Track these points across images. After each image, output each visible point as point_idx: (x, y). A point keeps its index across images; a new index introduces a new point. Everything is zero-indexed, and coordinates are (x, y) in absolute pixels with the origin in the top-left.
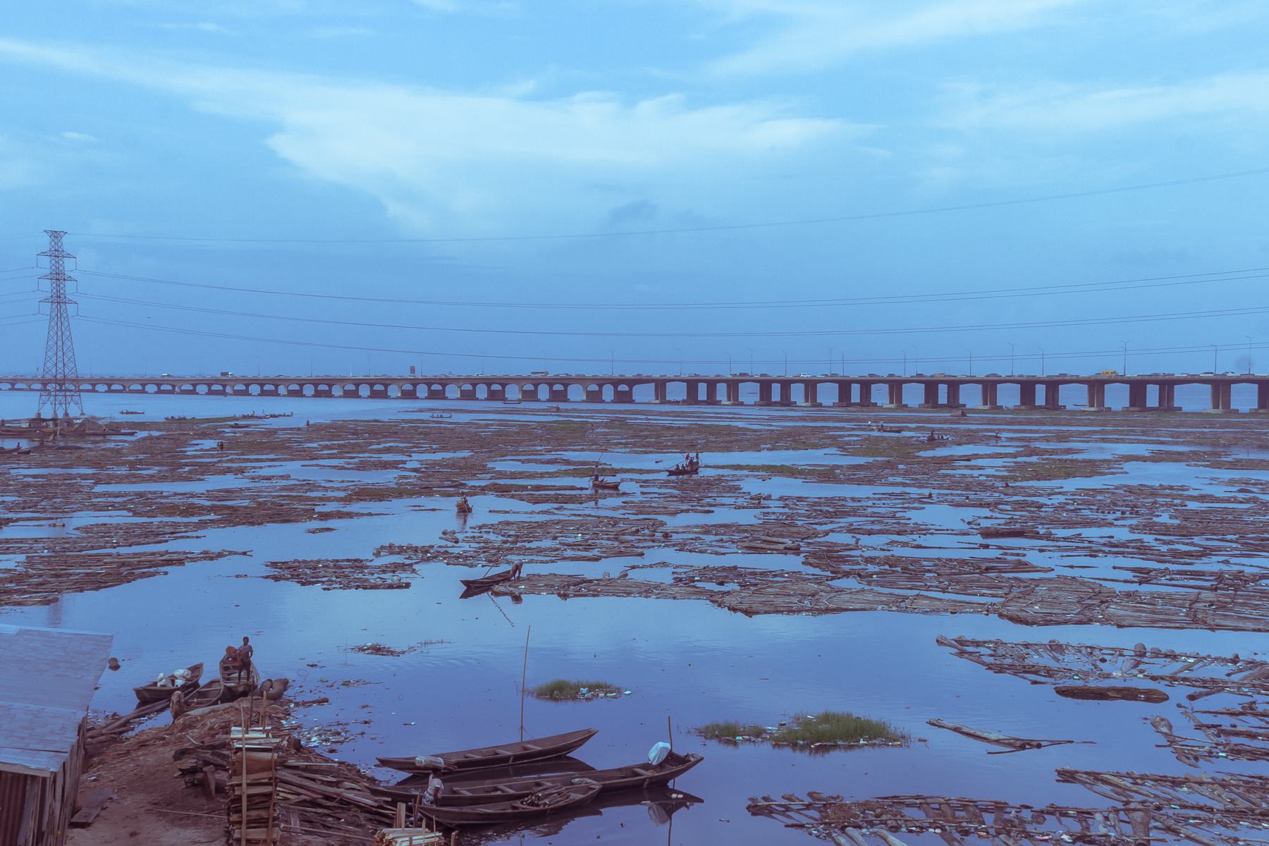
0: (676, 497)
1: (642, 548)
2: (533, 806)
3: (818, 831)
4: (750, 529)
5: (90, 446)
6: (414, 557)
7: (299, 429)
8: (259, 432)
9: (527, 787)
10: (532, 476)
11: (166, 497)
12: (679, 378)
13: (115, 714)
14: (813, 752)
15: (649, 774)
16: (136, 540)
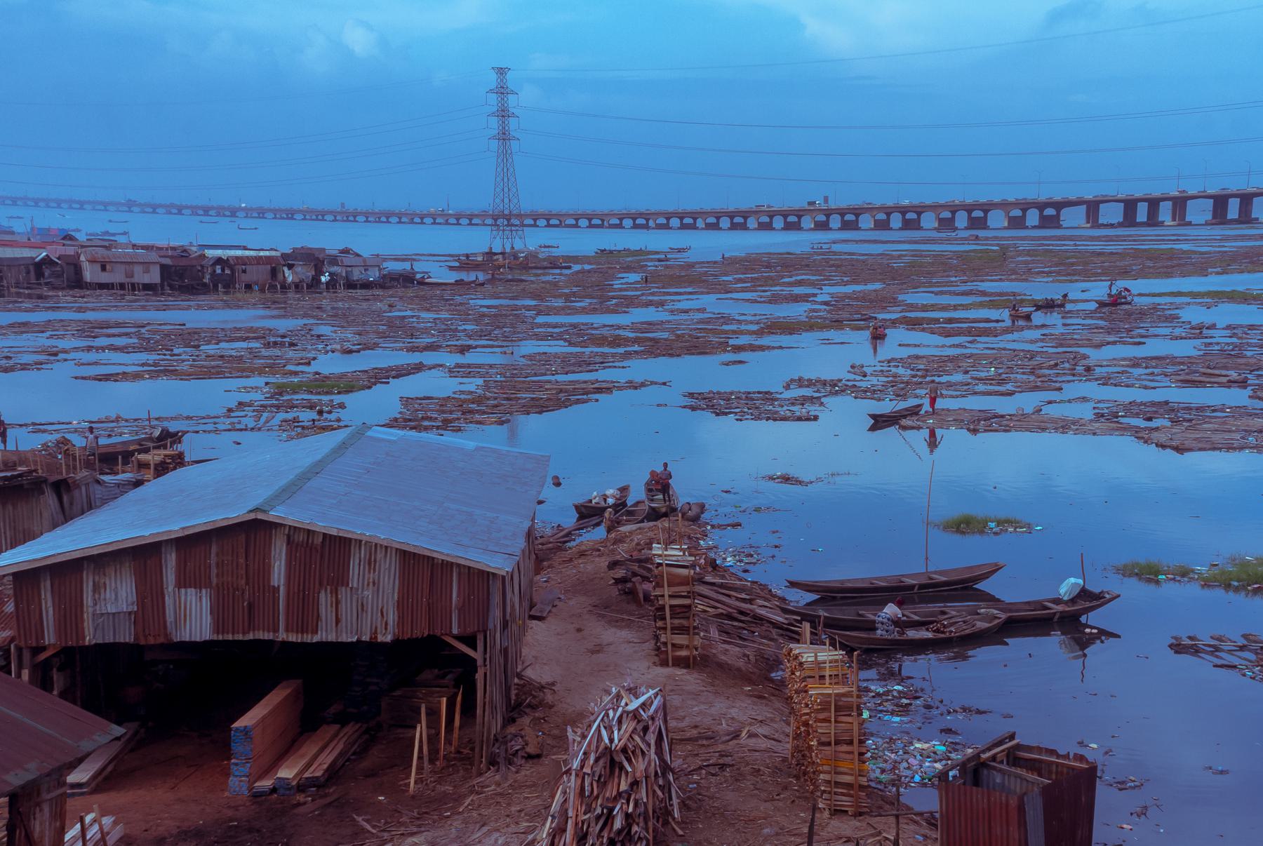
0: (1102, 328)
1: (1060, 382)
2: (938, 632)
3: (1253, 673)
4: (1189, 361)
5: (532, 279)
6: (823, 390)
7: (715, 262)
8: (678, 265)
9: (933, 614)
10: (944, 308)
11: (596, 329)
12: (1116, 198)
13: (559, 526)
14: (1250, 594)
15: (1060, 608)
16: (572, 368)
